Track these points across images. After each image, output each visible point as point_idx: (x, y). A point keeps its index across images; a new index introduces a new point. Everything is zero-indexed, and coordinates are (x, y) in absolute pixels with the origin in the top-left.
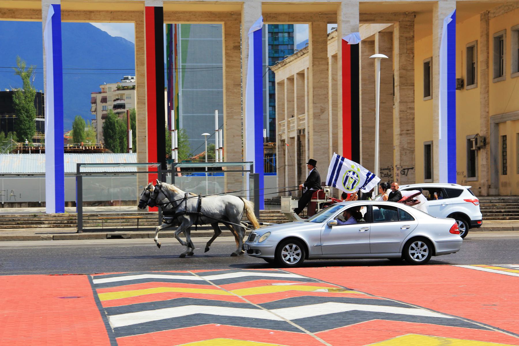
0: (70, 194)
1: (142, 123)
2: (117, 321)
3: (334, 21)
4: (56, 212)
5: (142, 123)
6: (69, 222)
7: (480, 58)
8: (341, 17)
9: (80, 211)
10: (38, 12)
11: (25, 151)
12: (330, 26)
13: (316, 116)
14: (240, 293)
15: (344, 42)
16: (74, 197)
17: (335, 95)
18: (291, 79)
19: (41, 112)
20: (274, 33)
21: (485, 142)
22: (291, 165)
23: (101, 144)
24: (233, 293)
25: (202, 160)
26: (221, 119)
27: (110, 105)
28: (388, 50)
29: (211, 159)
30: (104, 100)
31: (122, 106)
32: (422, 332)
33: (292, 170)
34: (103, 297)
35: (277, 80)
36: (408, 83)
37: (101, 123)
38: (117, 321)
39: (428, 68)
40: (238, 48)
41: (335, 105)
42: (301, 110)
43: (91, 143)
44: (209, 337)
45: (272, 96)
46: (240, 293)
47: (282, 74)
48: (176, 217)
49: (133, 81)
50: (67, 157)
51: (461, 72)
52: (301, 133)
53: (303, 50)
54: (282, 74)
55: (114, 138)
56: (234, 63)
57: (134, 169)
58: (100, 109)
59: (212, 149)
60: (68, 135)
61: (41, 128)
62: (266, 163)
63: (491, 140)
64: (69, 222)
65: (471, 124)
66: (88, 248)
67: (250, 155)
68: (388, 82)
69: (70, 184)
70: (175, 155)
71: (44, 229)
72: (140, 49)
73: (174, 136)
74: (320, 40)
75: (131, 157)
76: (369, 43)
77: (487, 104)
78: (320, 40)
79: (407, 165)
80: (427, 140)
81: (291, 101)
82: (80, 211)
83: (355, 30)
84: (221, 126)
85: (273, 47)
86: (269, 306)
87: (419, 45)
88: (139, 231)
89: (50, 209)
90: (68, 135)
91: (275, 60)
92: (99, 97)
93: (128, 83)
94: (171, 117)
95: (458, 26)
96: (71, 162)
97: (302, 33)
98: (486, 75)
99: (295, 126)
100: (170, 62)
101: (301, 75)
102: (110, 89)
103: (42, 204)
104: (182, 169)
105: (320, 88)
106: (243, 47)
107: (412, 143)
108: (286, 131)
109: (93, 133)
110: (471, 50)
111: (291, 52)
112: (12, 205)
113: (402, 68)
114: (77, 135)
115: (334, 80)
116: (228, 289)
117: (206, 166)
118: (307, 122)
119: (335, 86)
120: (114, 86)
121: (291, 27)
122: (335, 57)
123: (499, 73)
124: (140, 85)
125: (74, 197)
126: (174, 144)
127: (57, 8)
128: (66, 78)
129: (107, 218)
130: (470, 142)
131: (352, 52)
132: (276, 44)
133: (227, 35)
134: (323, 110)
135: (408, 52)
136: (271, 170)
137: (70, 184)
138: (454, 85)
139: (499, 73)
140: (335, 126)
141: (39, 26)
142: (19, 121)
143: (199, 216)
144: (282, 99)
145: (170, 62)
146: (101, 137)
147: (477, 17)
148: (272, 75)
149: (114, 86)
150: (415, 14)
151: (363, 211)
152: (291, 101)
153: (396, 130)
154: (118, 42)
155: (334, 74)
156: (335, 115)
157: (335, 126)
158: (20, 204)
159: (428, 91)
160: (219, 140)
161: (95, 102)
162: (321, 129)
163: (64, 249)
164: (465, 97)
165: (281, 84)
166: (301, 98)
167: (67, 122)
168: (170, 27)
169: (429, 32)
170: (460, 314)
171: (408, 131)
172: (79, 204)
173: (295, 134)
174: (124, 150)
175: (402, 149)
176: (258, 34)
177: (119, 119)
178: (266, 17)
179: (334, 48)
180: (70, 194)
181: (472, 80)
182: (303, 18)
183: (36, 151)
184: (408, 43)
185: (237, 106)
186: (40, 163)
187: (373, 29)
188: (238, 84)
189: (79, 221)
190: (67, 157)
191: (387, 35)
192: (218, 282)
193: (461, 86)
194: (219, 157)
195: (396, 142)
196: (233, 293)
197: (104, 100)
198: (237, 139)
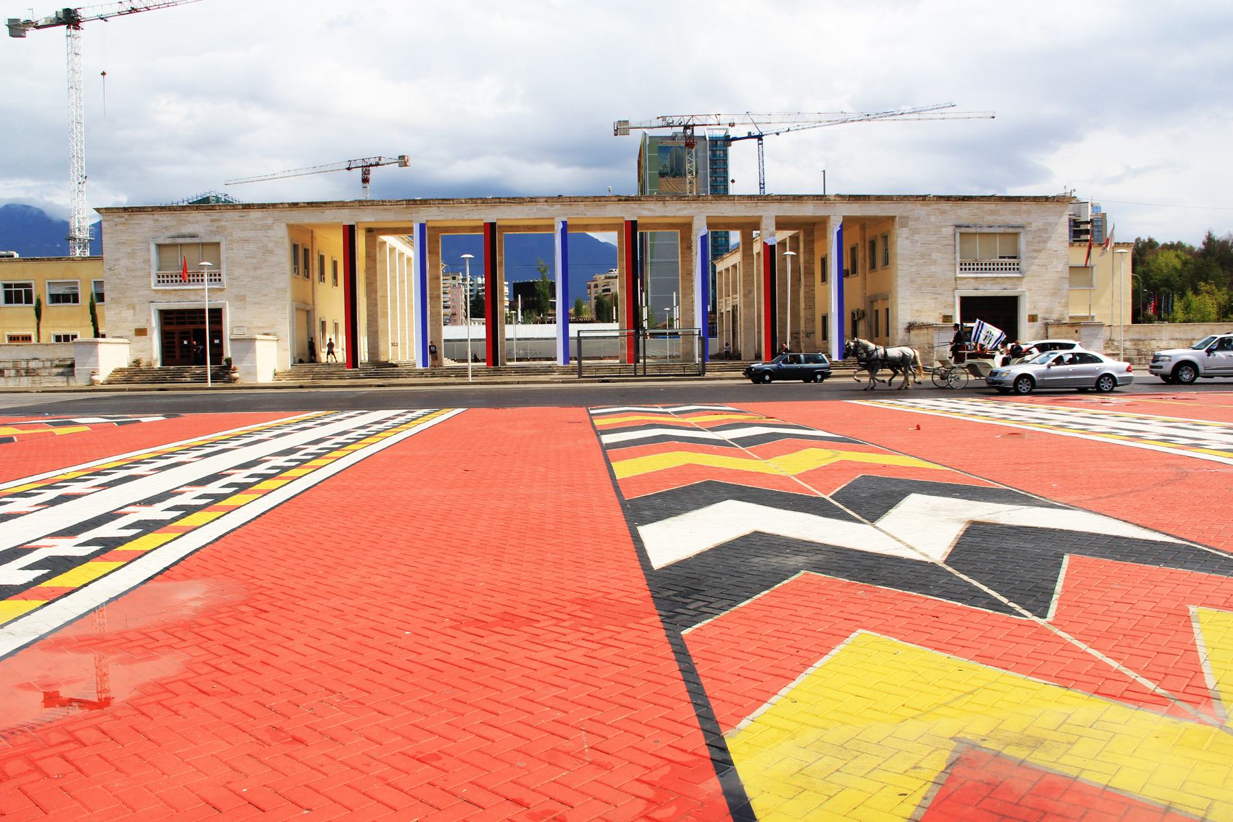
0: (573, 351)
1: (622, 301)
2: (607, 439)
3: (758, 229)
4: (946, 562)
5: (622, 301)
6: (573, 371)
7: (860, 255)
8: (763, 226)
9: (580, 363)
10: (552, 227)
11: (543, 322)
12: (755, 233)
13: (745, 296)
14: (692, 420)
15: (765, 244)
16: (576, 351)
17: (759, 281)
18: (727, 270)
19: (554, 296)
20: (715, 237)
21: (864, 314)
22: (728, 331)
23: (594, 317)
24: (687, 420)
25: (664, 327)
26: (678, 298)
27: (600, 290)
28: (795, 248)
29: (671, 326)
30: (596, 286)
31: (609, 290)
32: (820, 447)
33: (728, 335)
34: (597, 422)
35: (718, 270)
36: (810, 272)
37: (594, 302)
38: (607, 439)
39: (824, 262)
40: (689, 248)
41: (759, 288)
42: (735, 292)
43: (586, 317)
44: (671, 450)
45: (714, 282)
46: (692, 420)
47: (721, 266)
48: (871, 363)
49: (616, 272)
50: (571, 326)
51: (847, 265)
52: (735, 308)
53: (736, 249)
54: (721, 266)
55: (603, 313)
56: (688, 260)
57: (617, 334)
58: (593, 293)
59: (671, 320)
60: (572, 311)
61: (553, 306)
62: (710, 329)
63: (868, 312)
64: (573, 371)
65: (855, 301)
66: (586, 389)
67: (698, 323)
68: (796, 271)
69: (573, 345)
70: (645, 324)
71: (556, 376)
72: (621, 250)
73: (645, 310)
74: (748, 242)
75: (615, 326)
76: (782, 244)
77: (865, 288)
78: (748, 242)
79: (809, 330)
80: (824, 313)
81: (727, 285)
82: (580, 363)
83: (773, 235)
84: (678, 304)
85: (714, 247)
86: (713, 430)
87: (817, 246)
88: (620, 378)
89: (560, 362)
90: (572, 311)
91: (715, 257)
92: (593, 284)
93: (612, 274)
94: (642, 298)
95: (844, 233)
96: (574, 329)
97: (735, 237)
98: (864, 266)
99: (730, 303)
100: (642, 259)
101: (735, 266)
102: (600, 278)
103: (555, 359)
104: (652, 335)
105: (748, 276)
106: (694, 248)
107: (813, 314)
108: (724, 306)
109: (589, 308)
110: (853, 250)
111: (727, 251)
112: (534, 359)
113: (806, 262)
114: (578, 311)
115: (758, 270)
116: (766, 456)
117: (667, 331)
118: (739, 299)
119: (758, 274)
120: (603, 277)
121: (727, 233)
122: (758, 254)
123: (873, 266)
124: (621, 275)
125: (576, 351)
126: (645, 316)
127: (564, 223)
128: (570, 271)
129: (598, 368)
130: (853, 314)
131: (770, 251)
132: (717, 245)
133: (682, 239)
134: (751, 292)
135: (810, 251)
136: (714, 335)
137: (573, 345)
138: (842, 274)
139: (873, 266)
140: (759, 303)
141: (552, 237)
142: (539, 302)
143: (887, 362)
144: (721, 284)
145: (642, 259)
146: (594, 312)
147: (857, 228)
148: (714, 267)
149: (603, 277)
150: (814, 224)
151: (1066, 358)
152: (727, 285)
153: (802, 305)
154: (606, 246)
155: (758, 266)
156: (759, 295)
157: (759, 303)
158: (540, 359)
159: (824, 278)
160: (676, 314)
161: (589, 287)
162: (749, 304)
163: (570, 390)
164: (852, 283)
165: (721, 273)
166: (734, 283)
167: (571, 302)
168: (641, 234)
169: (824, 236)
170: (847, 434)
171: (811, 305)
172: (579, 358)
173: (730, 309)
174: (610, 320)
175: (806, 319)
176: (704, 238)
177: (607, 299)
178: (709, 226)
179: (757, 248)
180: (573, 351)
181: (854, 271)
182: (735, 226)
183: (550, 322)
184: (810, 244)
185: (689, 289)
186: (550, 331)
187: (785, 235)
188: (689, 273)
189: (580, 370)
190: (571, 326)
191: (795, 239)
192: (676, 413)
193: (847, 275)
194: (676, 324)
195: (802, 314)
196: (687, 420)
197: (596, 286)
198: (690, 312)
